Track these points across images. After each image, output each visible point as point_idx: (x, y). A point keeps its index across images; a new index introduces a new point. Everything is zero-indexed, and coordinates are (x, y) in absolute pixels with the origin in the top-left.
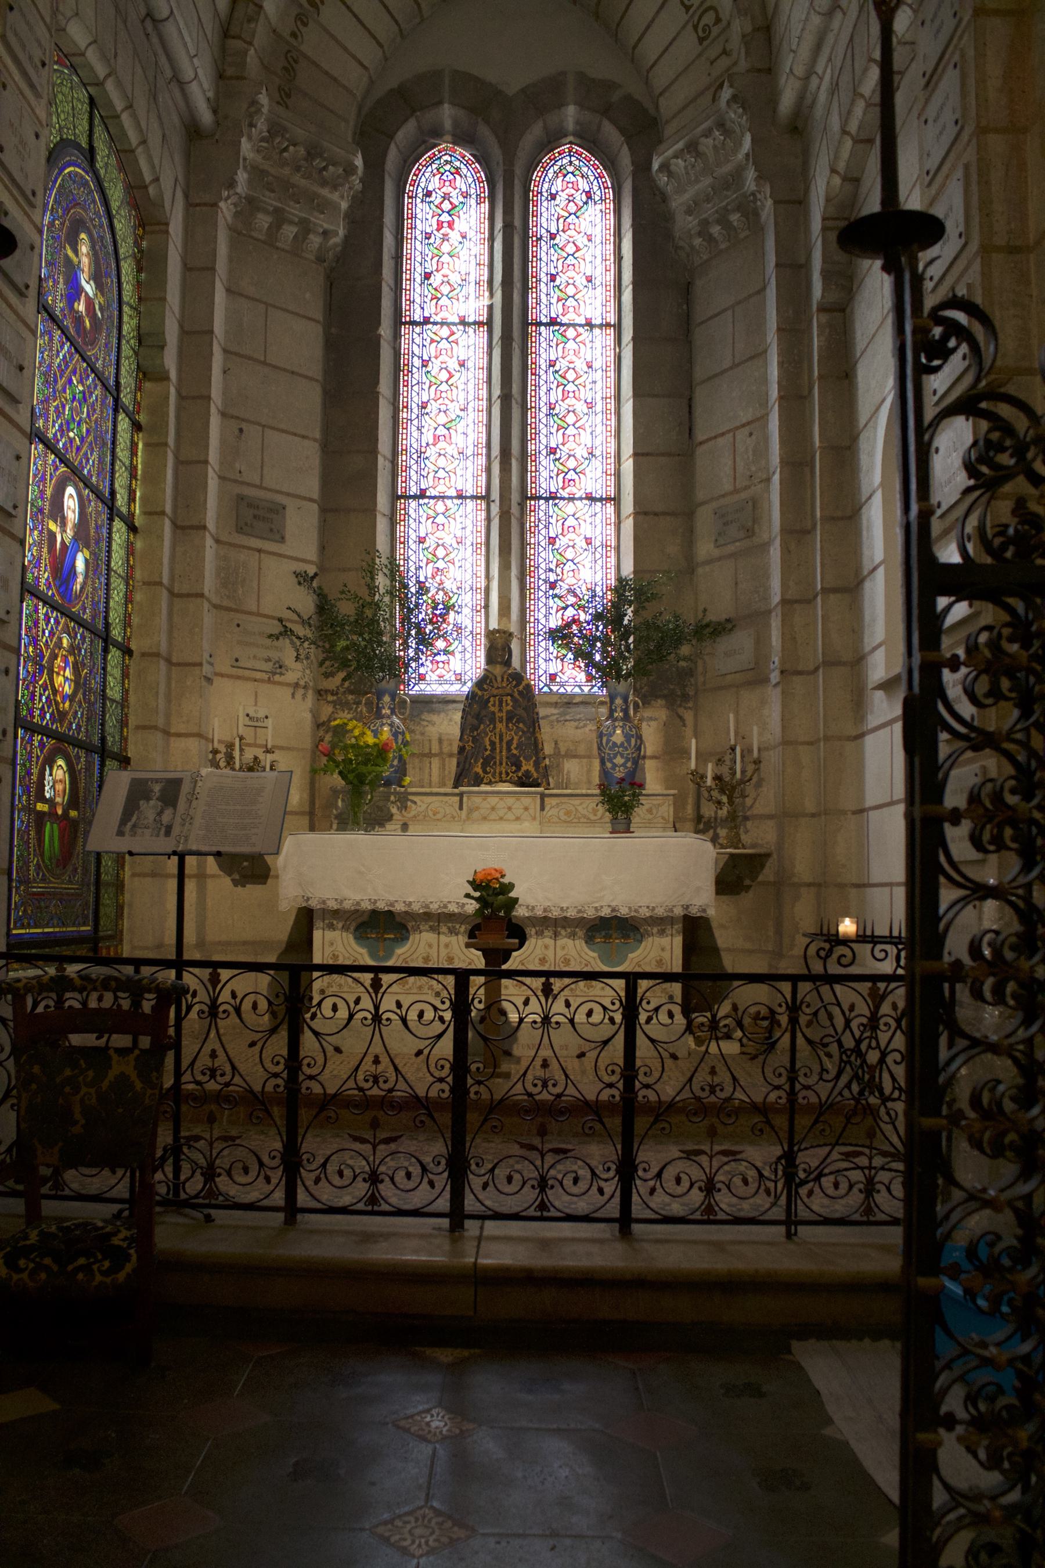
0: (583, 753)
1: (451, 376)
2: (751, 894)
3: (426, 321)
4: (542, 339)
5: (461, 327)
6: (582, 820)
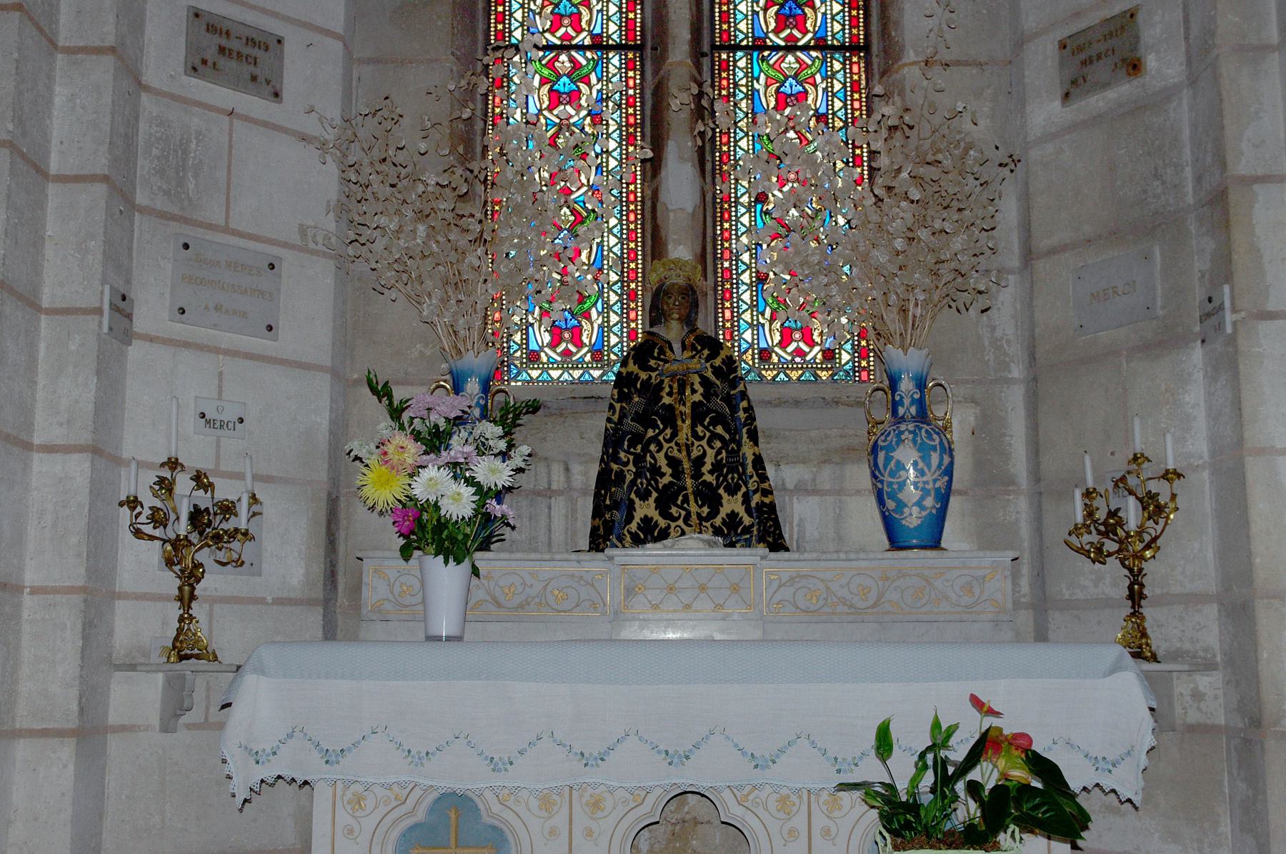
0: (827, 487)
6: (840, 608)
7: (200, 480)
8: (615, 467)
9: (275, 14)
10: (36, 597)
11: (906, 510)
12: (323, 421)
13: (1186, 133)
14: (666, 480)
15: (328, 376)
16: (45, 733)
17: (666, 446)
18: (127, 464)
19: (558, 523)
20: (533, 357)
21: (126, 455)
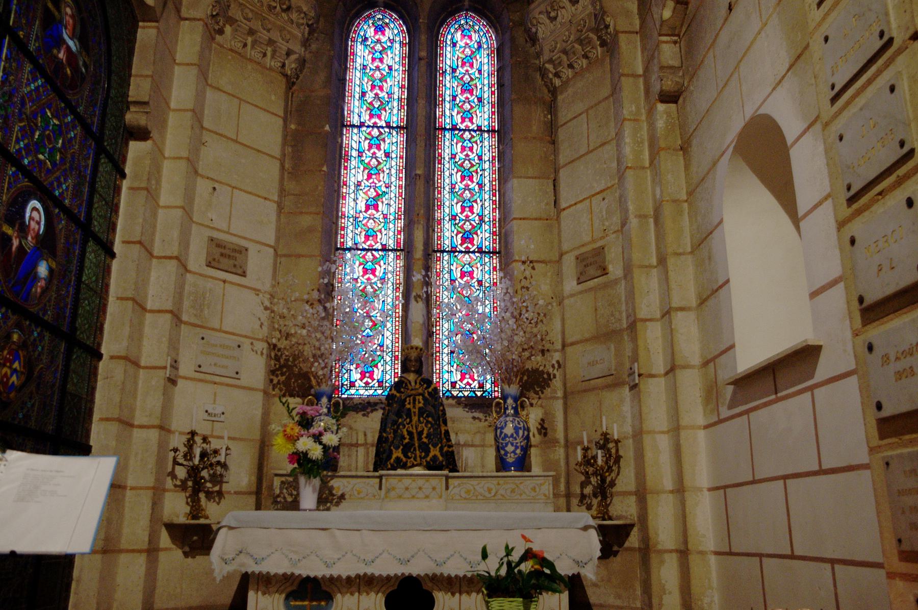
1: (379, 163)
2: (619, 558)
3: (362, 124)
4: (446, 140)
5: (387, 130)
6: (480, 497)
7: (205, 439)
8: (385, 435)
9: (245, 238)
10: (132, 491)
11: (509, 455)
12: (258, 413)
13: (623, 299)
14: (407, 441)
15: (262, 394)
16: (133, 551)
17: (407, 426)
18: (173, 432)
19: (361, 458)
20: (352, 384)
21: (173, 429)
